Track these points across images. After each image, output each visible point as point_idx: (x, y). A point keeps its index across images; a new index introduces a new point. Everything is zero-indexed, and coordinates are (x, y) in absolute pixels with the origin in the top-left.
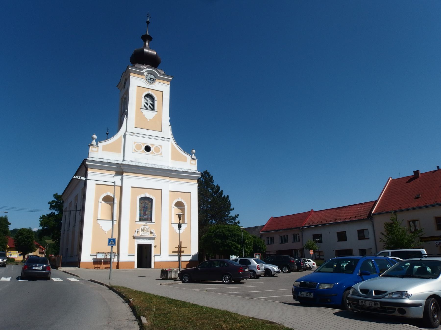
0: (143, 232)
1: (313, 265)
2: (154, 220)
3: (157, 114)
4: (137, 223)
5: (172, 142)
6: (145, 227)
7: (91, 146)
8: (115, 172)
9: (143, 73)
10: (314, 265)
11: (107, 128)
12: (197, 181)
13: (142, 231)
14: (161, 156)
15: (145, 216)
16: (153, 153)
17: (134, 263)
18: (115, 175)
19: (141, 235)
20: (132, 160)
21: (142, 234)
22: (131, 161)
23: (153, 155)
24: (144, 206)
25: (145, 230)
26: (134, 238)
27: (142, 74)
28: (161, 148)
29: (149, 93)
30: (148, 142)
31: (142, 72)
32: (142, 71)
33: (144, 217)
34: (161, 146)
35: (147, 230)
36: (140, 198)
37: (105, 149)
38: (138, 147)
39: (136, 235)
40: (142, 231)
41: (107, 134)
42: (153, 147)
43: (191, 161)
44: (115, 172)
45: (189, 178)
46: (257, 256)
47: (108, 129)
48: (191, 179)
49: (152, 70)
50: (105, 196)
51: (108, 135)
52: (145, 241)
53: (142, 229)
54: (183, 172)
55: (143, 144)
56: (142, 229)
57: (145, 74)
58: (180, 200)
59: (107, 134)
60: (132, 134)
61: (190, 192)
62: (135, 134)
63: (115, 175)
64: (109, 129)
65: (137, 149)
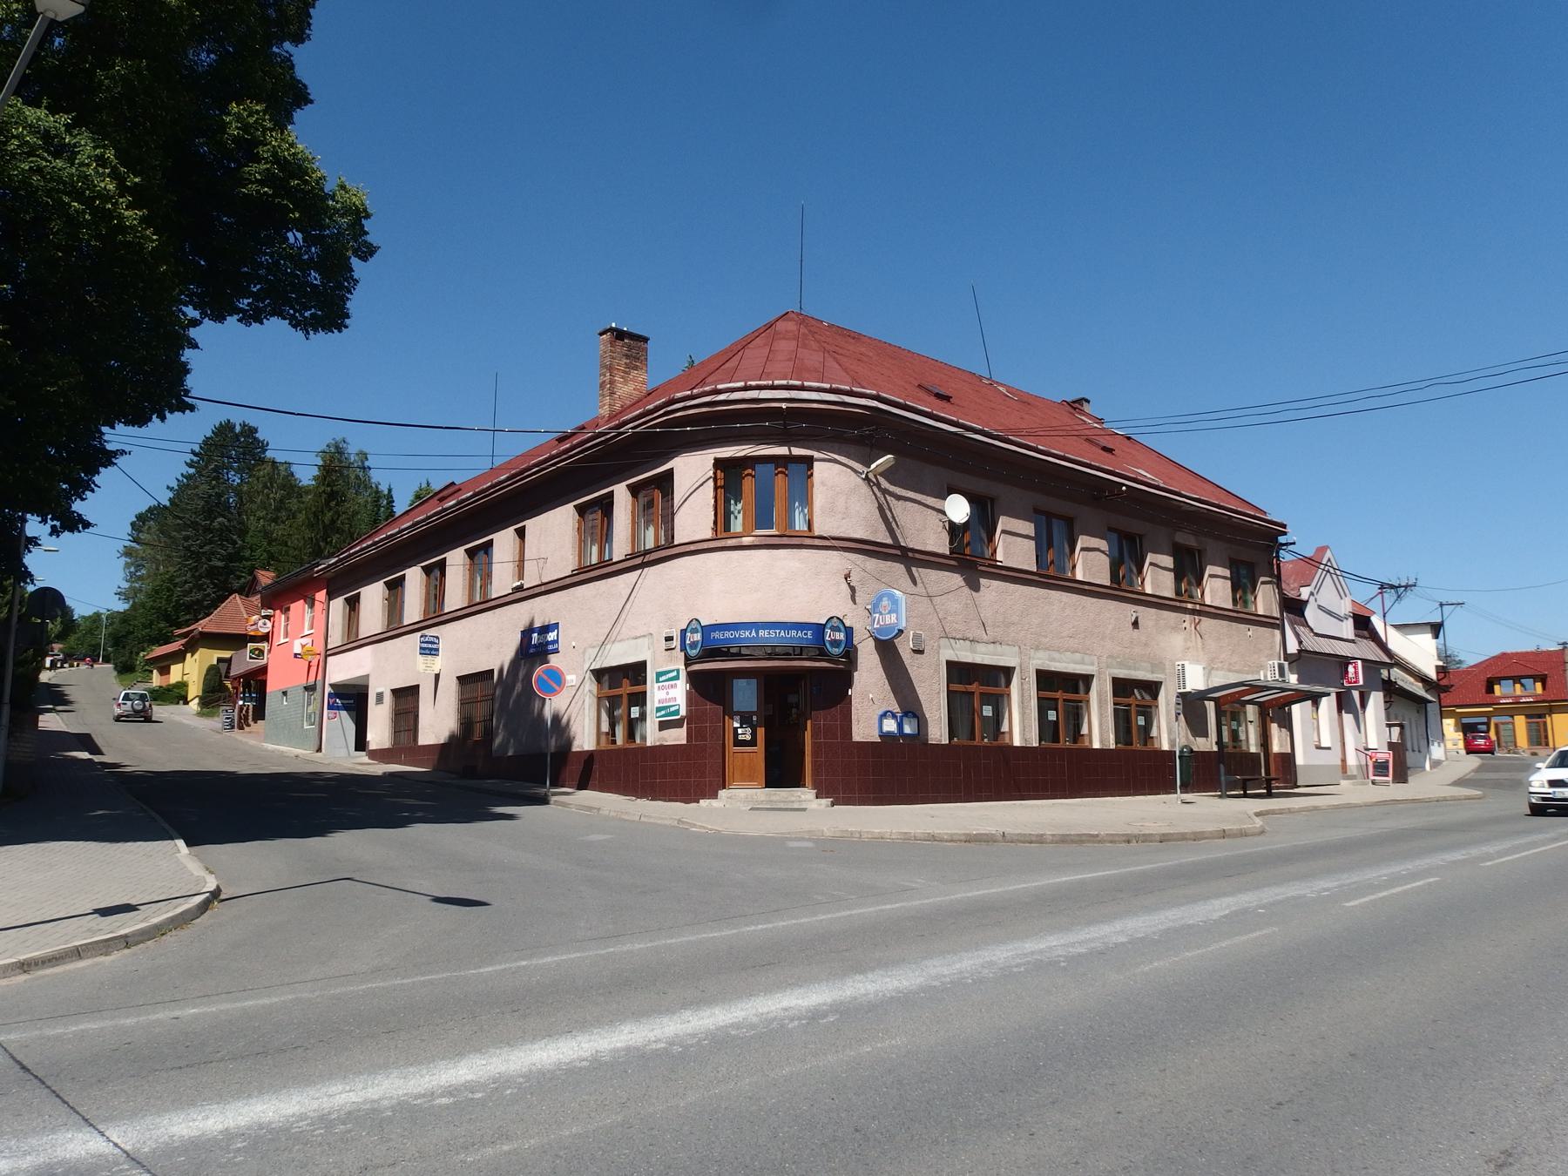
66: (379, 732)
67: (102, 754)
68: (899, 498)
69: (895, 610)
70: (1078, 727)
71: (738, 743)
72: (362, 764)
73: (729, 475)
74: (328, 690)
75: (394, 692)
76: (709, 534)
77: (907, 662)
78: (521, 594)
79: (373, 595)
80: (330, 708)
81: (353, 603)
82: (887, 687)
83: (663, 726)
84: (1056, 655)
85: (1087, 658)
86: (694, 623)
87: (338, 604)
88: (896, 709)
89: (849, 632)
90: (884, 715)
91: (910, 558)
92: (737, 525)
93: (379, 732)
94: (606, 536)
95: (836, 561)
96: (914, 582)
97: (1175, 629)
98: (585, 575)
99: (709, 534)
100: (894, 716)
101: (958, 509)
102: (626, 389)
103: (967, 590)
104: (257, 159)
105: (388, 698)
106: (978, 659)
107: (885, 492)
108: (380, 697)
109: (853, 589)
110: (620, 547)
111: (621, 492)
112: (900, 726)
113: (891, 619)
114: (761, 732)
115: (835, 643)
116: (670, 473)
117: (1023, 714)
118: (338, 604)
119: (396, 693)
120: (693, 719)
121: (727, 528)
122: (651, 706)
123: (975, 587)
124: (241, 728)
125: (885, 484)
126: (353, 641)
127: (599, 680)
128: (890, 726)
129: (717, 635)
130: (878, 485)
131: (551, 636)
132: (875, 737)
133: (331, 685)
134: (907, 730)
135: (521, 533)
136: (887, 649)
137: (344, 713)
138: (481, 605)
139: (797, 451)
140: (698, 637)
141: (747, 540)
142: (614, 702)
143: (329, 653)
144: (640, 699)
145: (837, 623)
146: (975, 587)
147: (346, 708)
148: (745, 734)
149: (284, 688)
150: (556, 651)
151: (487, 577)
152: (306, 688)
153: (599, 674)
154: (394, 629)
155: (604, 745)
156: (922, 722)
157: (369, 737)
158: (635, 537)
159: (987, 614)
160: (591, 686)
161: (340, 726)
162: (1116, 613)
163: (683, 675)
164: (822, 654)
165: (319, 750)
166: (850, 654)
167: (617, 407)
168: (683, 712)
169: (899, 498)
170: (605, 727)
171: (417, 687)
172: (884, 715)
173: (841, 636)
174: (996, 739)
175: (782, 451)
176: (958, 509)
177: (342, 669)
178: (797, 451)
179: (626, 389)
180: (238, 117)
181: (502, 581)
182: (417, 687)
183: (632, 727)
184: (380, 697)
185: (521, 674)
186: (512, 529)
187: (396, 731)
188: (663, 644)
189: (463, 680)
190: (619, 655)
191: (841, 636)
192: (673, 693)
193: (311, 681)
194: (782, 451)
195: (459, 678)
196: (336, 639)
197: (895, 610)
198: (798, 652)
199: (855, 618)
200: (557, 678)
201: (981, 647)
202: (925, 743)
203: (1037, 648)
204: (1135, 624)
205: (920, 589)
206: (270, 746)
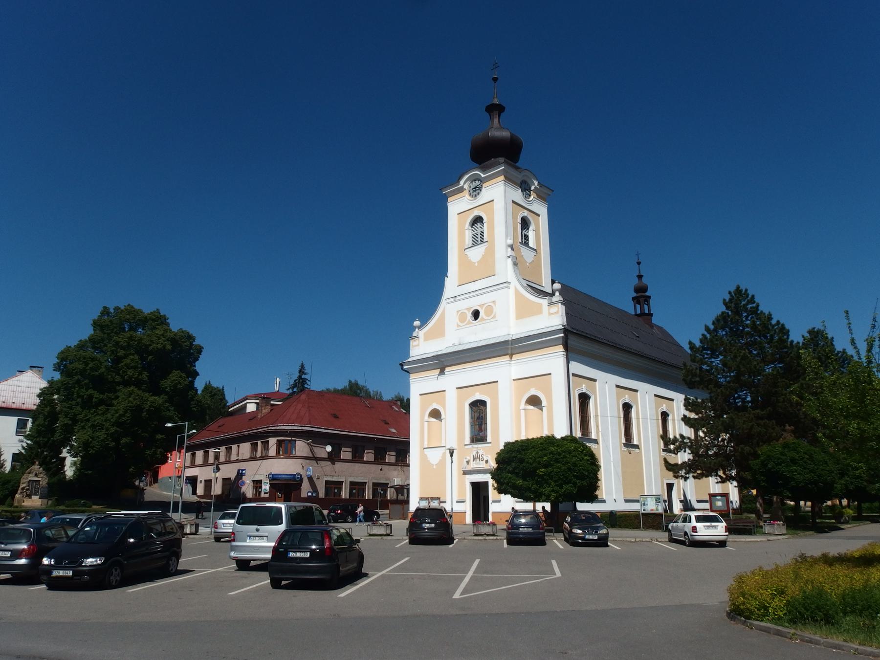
0: (475, 461)
1: (693, 532)
2: (489, 439)
3: (486, 246)
4: (467, 447)
5: (515, 288)
6: (478, 453)
7: (412, 339)
8: (439, 370)
9: (463, 187)
10: (697, 532)
11: (636, 253)
12: (560, 348)
13: (474, 459)
14: (495, 319)
15: (480, 434)
16: (483, 319)
17: (465, 515)
18: (439, 375)
19: (472, 467)
20: (455, 344)
21: (474, 465)
22: (454, 345)
23: (484, 322)
24: (479, 416)
25: (478, 458)
26: (465, 473)
27: (461, 190)
28: (461, 312)
29: (475, 216)
30: (474, 303)
31: (460, 186)
32: (459, 185)
33: (479, 434)
34: (458, 311)
35: (481, 457)
36: (470, 405)
37: (427, 338)
38: (462, 317)
39: (469, 468)
40: (474, 459)
41: (639, 263)
42: (482, 309)
43: (549, 309)
44: (439, 370)
45: (548, 345)
46: (719, 500)
47: (639, 253)
48: (552, 345)
49: (471, 175)
50: (530, 396)
51: (640, 266)
52: (481, 477)
53: (475, 456)
54: (529, 338)
55: (468, 309)
56: (475, 456)
57: (466, 186)
58: (533, 392)
59: (639, 263)
60: (452, 299)
61: (549, 373)
62: (457, 298)
63: (439, 375)
64: (636, 255)
65: (491, 314)
66: (200, 490)
67: (604, 501)
68: (314, 446)
69: (310, 472)
70: (386, 495)
71: (279, 497)
72: (194, 499)
73: (279, 443)
74: (185, 478)
75: (205, 480)
76: (275, 455)
77: (315, 481)
78: (238, 461)
79: (200, 454)
80: (185, 483)
81: (193, 455)
82: (310, 487)
83: (265, 493)
84: (356, 478)
85: (365, 478)
86: (270, 474)
87: (189, 454)
88: (311, 490)
89: (301, 475)
90: (308, 492)
91: (317, 459)
92: (281, 453)
93: (200, 490)
94: (256, 451)
95: (300, 461)
96: (318, 464)
97: (395, 470)
98: (253, 459)
99: (275, 455)
100: (311, 492)
101: (329, 448)
102: (265, 411)
103: (332, 465)
104: (193, 400)
105: (203, 482)
106: (334, 480)
107: (312, 446)
108: (201, 482)
109: (303, 467)
110: (259, 454)
111: (259, 442)
112: (312, 494)
113: (309, 473)
114: (283, 495)
115: (298, 478)
116: (268, 441)
117: (345, 492)
118: (189, 454)
119: (206, 481)
120: (270, 492)
121: (279, 453)
122: (263, 489)
123: (334, 464)
124: (150, 486)
125: (312, 444)
126: (193, 465)
127: (254, 483)
128: (310, 494)
129: (275, 476)
130: (310, 445)
131: (244, 472)
132: (306, 496)
133: (186, 477)
134: (314, 495)
135: (239, 446)
136: (310, 479)
137: (189, 485)
138: (228, 461)
139: (293, 439)
140: (271, 476)
141: (282, 457)
142: (256, 487)
143: (185, 468)
144: (261, 487)
145: (298, 474)
146: (334, 464)
147: (189, 483)
148: (280, 495)
149: (170, 476)
150: (245, 475)
151: (230, 454)
152: (178, 477)
153: (254, 481)
154: (206, 463)
155: (254, 497)
156: (318, 493)
157: (197, 492)
158: (262, 452)
159: (337, 470)
160: (252, 484)
161: (187, 489)
162: (376, 468)
163: (269, 483)
164: (295, 480)
165: (457, 502)
166: (301, 480)
167: (263, 416)
168: (268, 491)
169: (315, 447)
170: (254, 493)
171: (211, 480)
172: (308, 492)
173: (299, 476)
174: (363, 497)
175: (290, 439)
176: (329, 448)
177: (190, 472)
178: (293, 439)
179: (265, 411)
180: (191, 394)
181: (234, 457)
182: (211, 480)
183: (260, 493)
184: (201, 482)
185: (236, 482)
186: (236, 445)
187: (205, 490)
188: (265, 476)
189: (223, 479)
190: (257, 478)
191: (299, 476)
192: (266, 487)
193: (180, 474)
194: (290, 439)
195: (223, 479)
196: (188, 464)
197: (310, 472)
198: (290, 480)
199: (302, 472)
200: (244, 483)
201: (335, 477)
202: (318, 498)
203: (350, 477)
204: (381, 470)
205: (319, 465)
206: (166, 493)
